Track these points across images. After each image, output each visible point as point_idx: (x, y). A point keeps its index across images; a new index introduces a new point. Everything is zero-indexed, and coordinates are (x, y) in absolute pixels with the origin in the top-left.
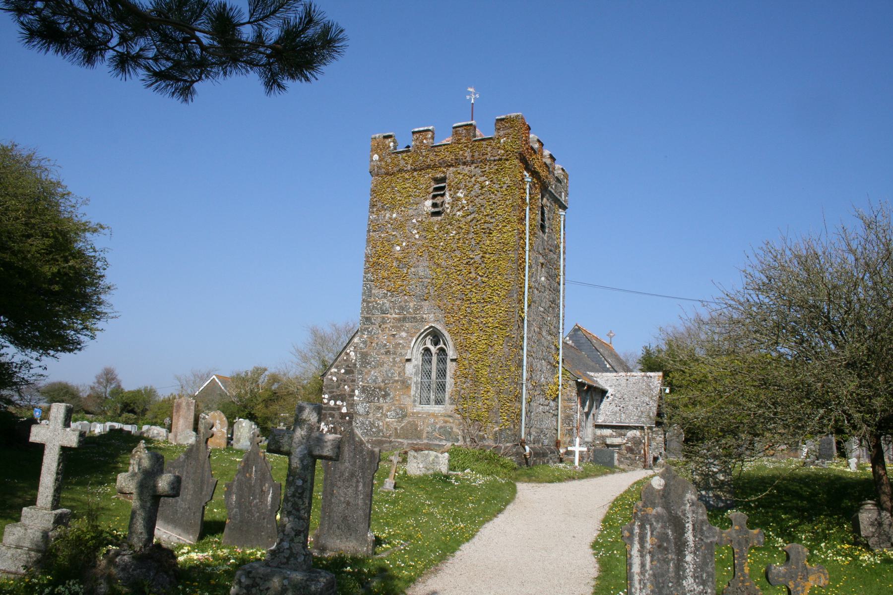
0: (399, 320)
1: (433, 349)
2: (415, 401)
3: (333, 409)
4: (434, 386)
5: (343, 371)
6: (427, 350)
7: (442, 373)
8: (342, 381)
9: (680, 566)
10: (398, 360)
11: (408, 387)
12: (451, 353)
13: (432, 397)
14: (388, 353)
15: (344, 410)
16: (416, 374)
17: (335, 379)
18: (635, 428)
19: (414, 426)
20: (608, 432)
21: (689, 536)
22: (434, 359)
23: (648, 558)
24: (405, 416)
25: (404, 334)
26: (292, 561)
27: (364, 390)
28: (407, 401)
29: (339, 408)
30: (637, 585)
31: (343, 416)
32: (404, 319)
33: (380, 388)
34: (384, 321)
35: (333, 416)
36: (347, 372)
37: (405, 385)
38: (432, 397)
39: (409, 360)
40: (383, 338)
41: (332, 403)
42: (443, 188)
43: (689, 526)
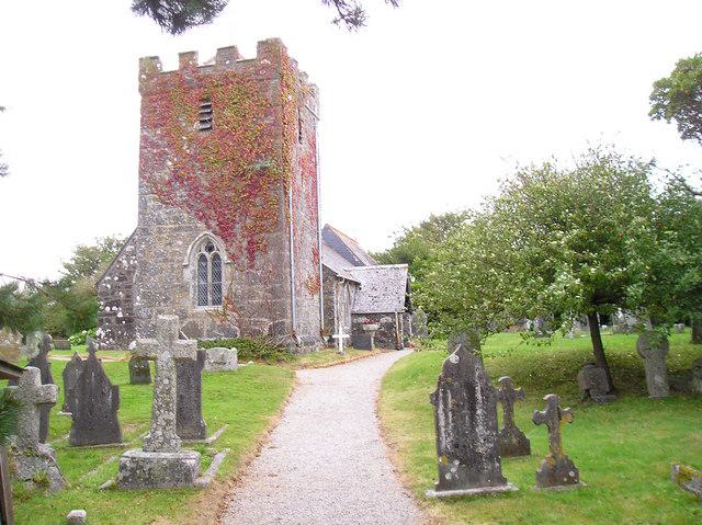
0: (175, 230)
1: (209, 256)
2: (194, 303)
3: (109, 315)
4: (210, 289)
5: (116, 278)
6: (203, 256)
7: (217, 275)
8: (115, 288)
9: (473, 418)
10: (176, 266)
11: (187, 290)
12: (224, 257)
13: (210, 298)
14: (166, 260)
15: (120, 315)
16: (194, 278)
17: (109, 286)
18: (387, 314)
19: (194, 325)
20: (363, 319)
21: (479, 396)
22: (210, 264)
23: (450, 415)
24: (186, 317)
25: (180, 243)
26: (166, 445)
27: (144, 296)
28: (188, 304)
29: (115, 314)
30: (443, 435)
31: (119, 321)
32: (179, 229)
33: (161, 294)
34: (160, 231)
35: (109, 321)
36: (120, 280)
37: (184, 288)
38: (210, 298)
39: (186, 266)
40: (160, 248)
41: (108, 309)
42: (209, 106)
43: (478, 388)
